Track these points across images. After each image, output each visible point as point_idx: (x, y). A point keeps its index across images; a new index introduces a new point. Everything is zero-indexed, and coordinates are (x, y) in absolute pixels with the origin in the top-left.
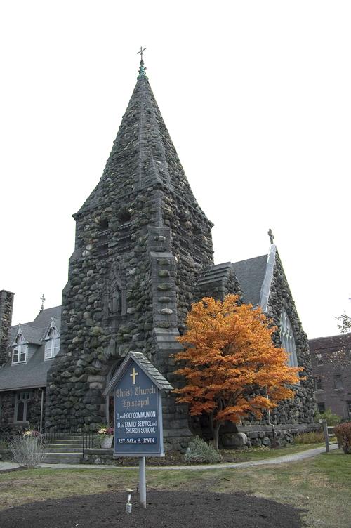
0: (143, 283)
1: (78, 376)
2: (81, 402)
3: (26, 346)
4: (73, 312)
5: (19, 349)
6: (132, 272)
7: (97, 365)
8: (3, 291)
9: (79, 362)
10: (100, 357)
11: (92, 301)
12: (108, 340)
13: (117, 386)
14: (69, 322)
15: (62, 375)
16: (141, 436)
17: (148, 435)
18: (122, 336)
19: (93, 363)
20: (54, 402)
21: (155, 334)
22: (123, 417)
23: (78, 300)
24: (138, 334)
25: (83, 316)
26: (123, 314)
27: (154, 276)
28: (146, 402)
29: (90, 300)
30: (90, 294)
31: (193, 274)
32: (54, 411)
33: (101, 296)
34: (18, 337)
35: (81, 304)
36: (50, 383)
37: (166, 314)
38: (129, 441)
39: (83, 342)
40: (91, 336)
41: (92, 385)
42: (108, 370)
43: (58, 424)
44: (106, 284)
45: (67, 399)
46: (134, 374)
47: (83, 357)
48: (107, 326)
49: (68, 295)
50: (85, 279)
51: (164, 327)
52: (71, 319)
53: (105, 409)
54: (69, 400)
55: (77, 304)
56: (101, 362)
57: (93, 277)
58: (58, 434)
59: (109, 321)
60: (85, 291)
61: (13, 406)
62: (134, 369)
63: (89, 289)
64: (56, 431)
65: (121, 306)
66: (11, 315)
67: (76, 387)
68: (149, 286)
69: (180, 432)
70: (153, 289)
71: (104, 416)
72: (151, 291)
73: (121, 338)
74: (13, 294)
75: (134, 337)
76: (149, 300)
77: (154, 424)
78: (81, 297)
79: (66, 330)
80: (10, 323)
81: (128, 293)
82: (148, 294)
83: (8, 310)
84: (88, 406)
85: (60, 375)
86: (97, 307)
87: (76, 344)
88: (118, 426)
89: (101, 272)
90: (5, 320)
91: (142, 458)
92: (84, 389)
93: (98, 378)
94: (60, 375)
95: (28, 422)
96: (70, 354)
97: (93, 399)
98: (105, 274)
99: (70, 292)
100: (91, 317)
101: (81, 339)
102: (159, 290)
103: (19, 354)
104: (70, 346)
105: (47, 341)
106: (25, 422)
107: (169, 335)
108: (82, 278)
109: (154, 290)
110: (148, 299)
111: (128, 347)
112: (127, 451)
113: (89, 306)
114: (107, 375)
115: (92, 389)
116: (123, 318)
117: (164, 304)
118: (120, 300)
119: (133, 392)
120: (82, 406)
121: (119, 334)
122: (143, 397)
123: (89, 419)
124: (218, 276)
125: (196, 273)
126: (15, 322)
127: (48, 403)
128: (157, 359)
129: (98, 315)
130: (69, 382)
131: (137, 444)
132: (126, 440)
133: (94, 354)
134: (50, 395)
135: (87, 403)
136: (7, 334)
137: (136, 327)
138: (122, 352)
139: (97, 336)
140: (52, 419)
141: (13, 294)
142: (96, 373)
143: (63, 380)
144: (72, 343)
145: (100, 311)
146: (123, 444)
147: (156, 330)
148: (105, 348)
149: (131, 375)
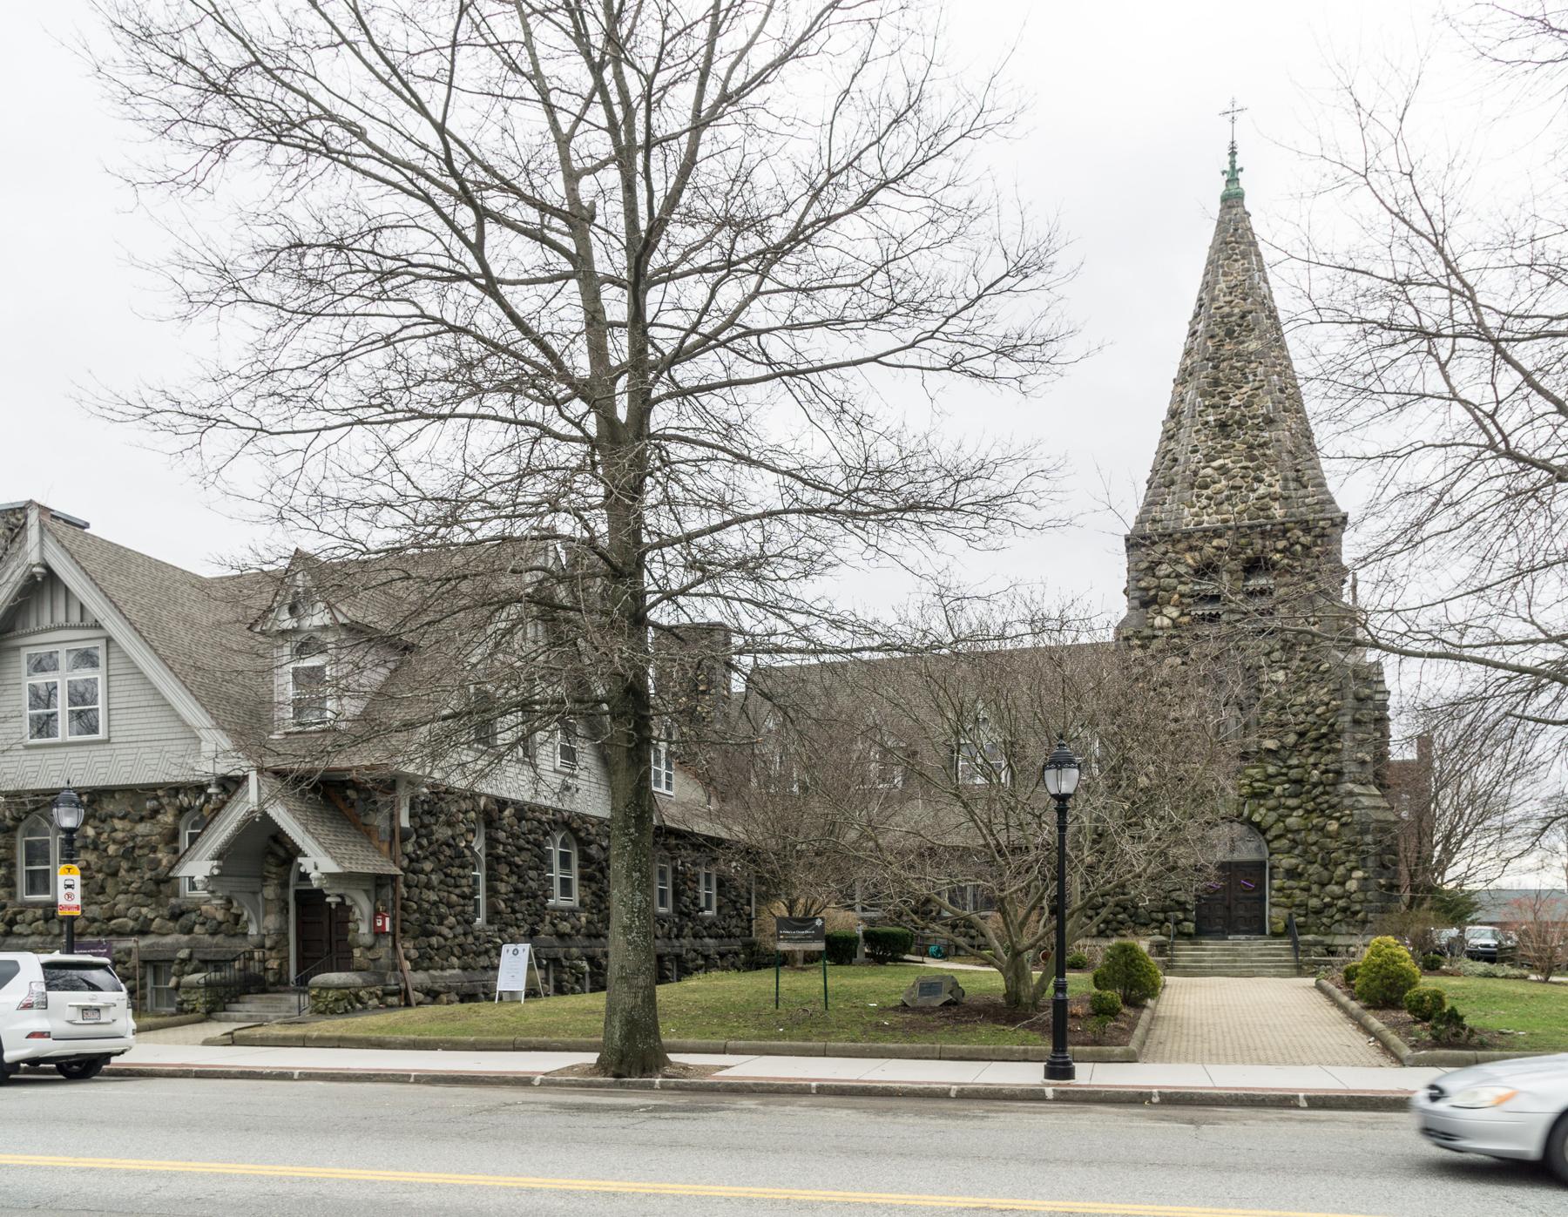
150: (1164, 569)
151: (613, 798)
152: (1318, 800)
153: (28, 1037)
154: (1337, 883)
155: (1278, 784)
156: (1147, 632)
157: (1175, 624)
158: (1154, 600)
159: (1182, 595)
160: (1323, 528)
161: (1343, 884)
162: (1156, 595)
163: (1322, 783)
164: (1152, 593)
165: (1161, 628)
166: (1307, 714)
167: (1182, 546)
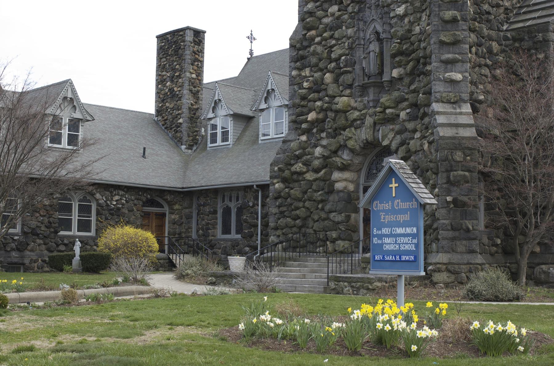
0: (417, 29)
1: (317, 171)
2: (323, 209)
3: (230, 119)
4: (307, 72)
5: (219, 122)
6: (401, 10)
7: (346, 156)
8: (188, 28)
9: (318, 151)
10: (351, 143)
11: (337, 56)
12: (362, 119)
13: (374, 197)
14: (301, 87)
15: (293, 169)
16: (401, 253)
17: (407, 253)
18: (383, 112)
19: (340, 153)
20: (281, 209)
21: (435, 113)
22: (380, 233)
23: (314, 53)
24: (408, 111)
25: (323, 79)
26: (386, 78)
27: (435, 21)
28: (406, 217)
29: (333, 56)
30: (334, 45)
31: (502, 10)
32: (282, 222)
33: (351, 48)
34: (217, 103)
35: (320, 60)
36: (275, 181)
37: (452, 82)
38: (387, 258)
39: (323, 121)
40: (337, 112)
41: (339, 186)
42: (362, 164)
43: (287, 241)
44: (359, 30)
45: (301, 204)
46: (394, 185)
47: (324, 142)
48: (361, 96)
49: (298, 45)
50: (326, 20)
51: (449, 102)
52: (305, 84)
53: (357, 222)
54: (304, 207)
55: (314, 60)
56: (352, 151)
57: (338, 18)
58: (290, 254)
59: (364, 89)
60: (326, 39)
61: (215, 212)
62: (393, 179)
63: (332, 37)
64: (285, 250)
65: (382, 65)
66: (202, 67)
67: (314, 187)
68: (425, 35)
69: (467, 257)
70: (432, 42)
71: (355, 230)
72: (429, 44)
73: (382, 116)
74: (204, 32)
75: (403, 115)
76: (427, 59)
77: (415, 241)
78: (319, 49)
79: (297, 101)
80: (201, 80)
81: (394, 46)
82: (425, 48)
83: (197, 60)
84: (332, 215)
85: (289, 170)
86: (346, 66)
87: (313, 123)
88: (375, 242)
89: (350, 9)
90: (194, 76)
91: (400, 276)
92: (326, 190)
93: (347, 175)
94: (289, 170)
95: (239, 236)
96: (304, 138)
97: (340, 206)
98: (357, 13)
99: (301, 41)
100: (336, 81)
101: (321, 116)
102: (442, 43)
103: (219, 131)
104: (304, 126)
105: (262, 110)
106: (234, 236)
107: (456, 114)
108: (320, 19)
109: (435, 43)
110: (425, 57)
111: (393, 130)
112: (383, 268)
113: (333, 65)
114: (361, 169)
115: (339, 191)
116: (385, 84)
117: (449, 66)
118: (381, 53)
119: (393, 204)
120: (323, 215)
121: (378, 109)
122: (402, 212)
123: (334, 235)
124: (544, 13)
125: (506, 9)
126: (209, 77)
127: (274, 210)
128: (437, 151)
129: (347, 79)
130: (304, 179)
131: (396, 261)
132: (383, 257)
133: (341, 139)
134: (276, 198)
135: (331, 212)
136: (198, 99)
137: (406, 100)
138: (384, 137)
139: (345, 112)
140: (279, 232)
141: (204, 32)
142: (344, 168)
143: (295, 177)
144: (306, 121)
145: (350, 72)
146: (380, 261)
147: (436, 107)
148: (359, 131)
149: (390, 186)
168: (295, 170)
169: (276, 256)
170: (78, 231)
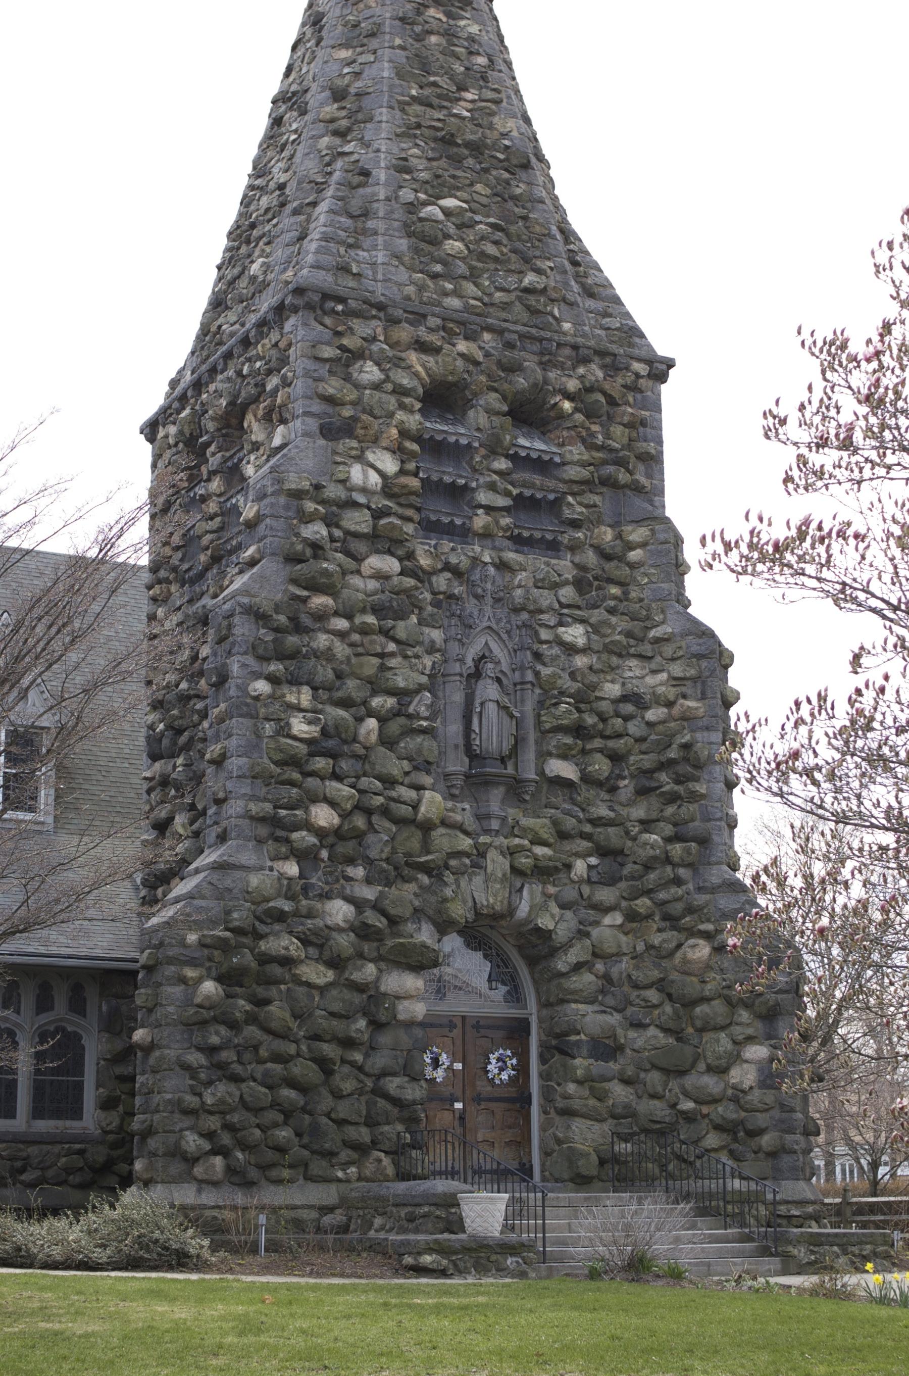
23: (327, 655)
75: (580, 867)
150: (370, 372)
151: (531, 425)
152: (662, 895)
153: (904, 677)
154: (710, 1069)
155: (577, 855)
156: (333, 491)
157: (389, 488)
158: (347, 429)
159: (404, 433)
160: (638, 376)
161: (721, 1071)
162: (354, 419)
163: (667, 860)
164: (347, 412)
165: (364, 490)
166: (627, 718)
167: (404, 333)
168: (283, 952)
169: (706, 1190)
170: (14, 1116)
